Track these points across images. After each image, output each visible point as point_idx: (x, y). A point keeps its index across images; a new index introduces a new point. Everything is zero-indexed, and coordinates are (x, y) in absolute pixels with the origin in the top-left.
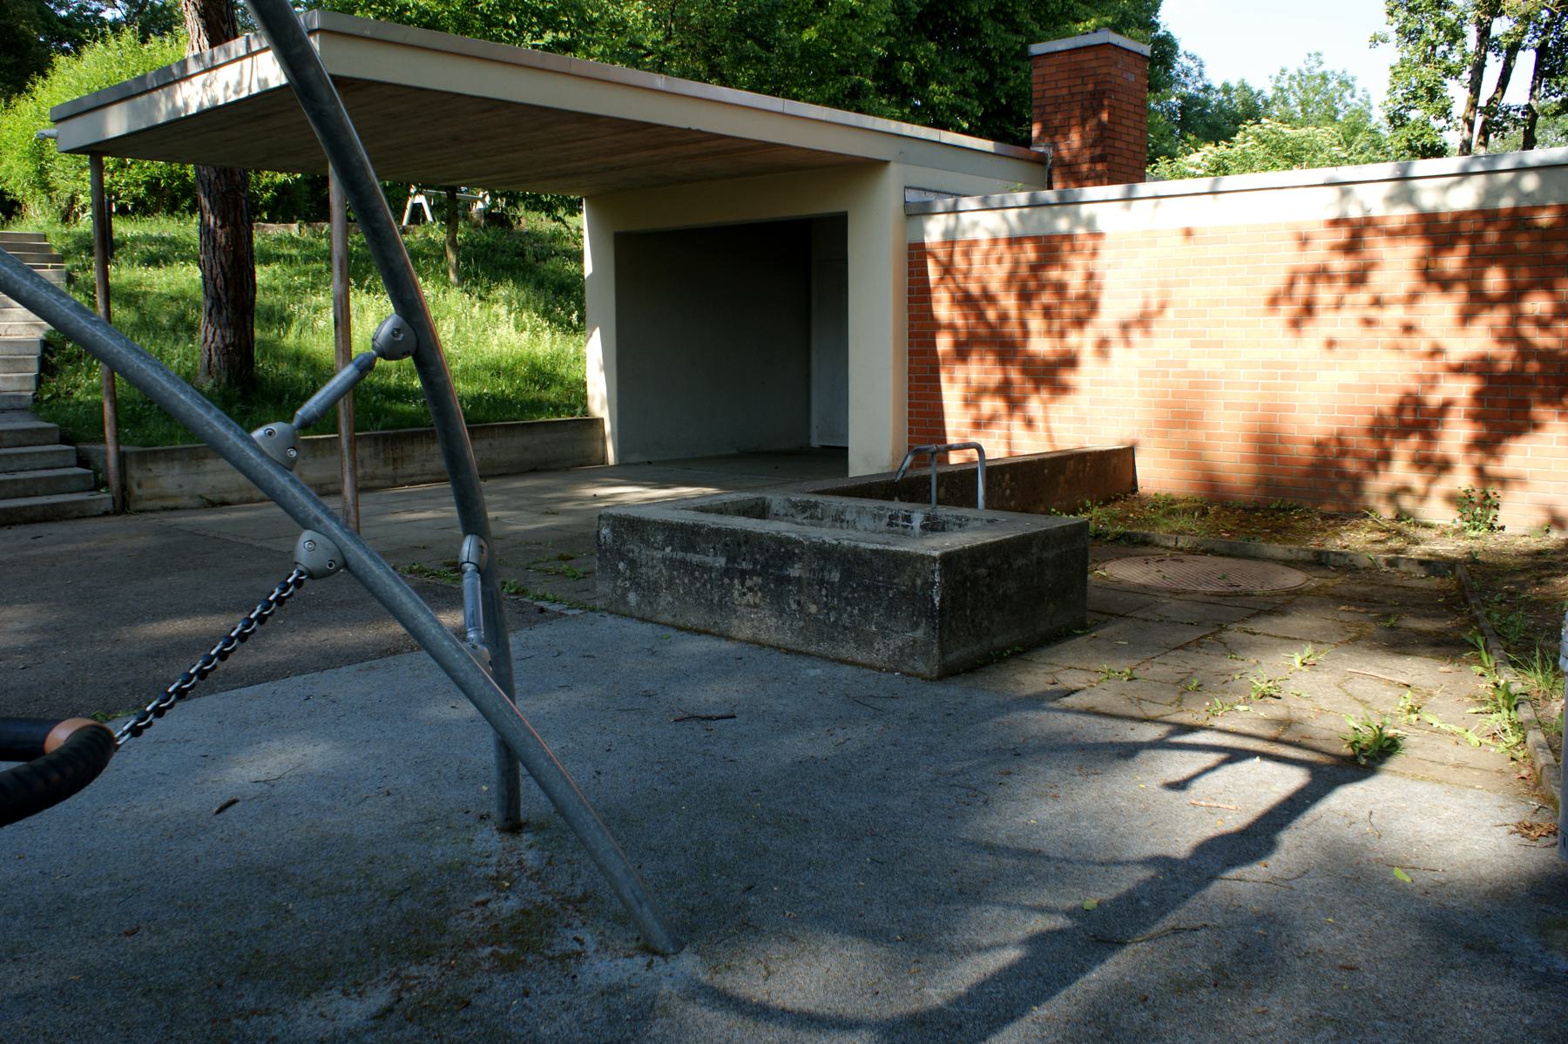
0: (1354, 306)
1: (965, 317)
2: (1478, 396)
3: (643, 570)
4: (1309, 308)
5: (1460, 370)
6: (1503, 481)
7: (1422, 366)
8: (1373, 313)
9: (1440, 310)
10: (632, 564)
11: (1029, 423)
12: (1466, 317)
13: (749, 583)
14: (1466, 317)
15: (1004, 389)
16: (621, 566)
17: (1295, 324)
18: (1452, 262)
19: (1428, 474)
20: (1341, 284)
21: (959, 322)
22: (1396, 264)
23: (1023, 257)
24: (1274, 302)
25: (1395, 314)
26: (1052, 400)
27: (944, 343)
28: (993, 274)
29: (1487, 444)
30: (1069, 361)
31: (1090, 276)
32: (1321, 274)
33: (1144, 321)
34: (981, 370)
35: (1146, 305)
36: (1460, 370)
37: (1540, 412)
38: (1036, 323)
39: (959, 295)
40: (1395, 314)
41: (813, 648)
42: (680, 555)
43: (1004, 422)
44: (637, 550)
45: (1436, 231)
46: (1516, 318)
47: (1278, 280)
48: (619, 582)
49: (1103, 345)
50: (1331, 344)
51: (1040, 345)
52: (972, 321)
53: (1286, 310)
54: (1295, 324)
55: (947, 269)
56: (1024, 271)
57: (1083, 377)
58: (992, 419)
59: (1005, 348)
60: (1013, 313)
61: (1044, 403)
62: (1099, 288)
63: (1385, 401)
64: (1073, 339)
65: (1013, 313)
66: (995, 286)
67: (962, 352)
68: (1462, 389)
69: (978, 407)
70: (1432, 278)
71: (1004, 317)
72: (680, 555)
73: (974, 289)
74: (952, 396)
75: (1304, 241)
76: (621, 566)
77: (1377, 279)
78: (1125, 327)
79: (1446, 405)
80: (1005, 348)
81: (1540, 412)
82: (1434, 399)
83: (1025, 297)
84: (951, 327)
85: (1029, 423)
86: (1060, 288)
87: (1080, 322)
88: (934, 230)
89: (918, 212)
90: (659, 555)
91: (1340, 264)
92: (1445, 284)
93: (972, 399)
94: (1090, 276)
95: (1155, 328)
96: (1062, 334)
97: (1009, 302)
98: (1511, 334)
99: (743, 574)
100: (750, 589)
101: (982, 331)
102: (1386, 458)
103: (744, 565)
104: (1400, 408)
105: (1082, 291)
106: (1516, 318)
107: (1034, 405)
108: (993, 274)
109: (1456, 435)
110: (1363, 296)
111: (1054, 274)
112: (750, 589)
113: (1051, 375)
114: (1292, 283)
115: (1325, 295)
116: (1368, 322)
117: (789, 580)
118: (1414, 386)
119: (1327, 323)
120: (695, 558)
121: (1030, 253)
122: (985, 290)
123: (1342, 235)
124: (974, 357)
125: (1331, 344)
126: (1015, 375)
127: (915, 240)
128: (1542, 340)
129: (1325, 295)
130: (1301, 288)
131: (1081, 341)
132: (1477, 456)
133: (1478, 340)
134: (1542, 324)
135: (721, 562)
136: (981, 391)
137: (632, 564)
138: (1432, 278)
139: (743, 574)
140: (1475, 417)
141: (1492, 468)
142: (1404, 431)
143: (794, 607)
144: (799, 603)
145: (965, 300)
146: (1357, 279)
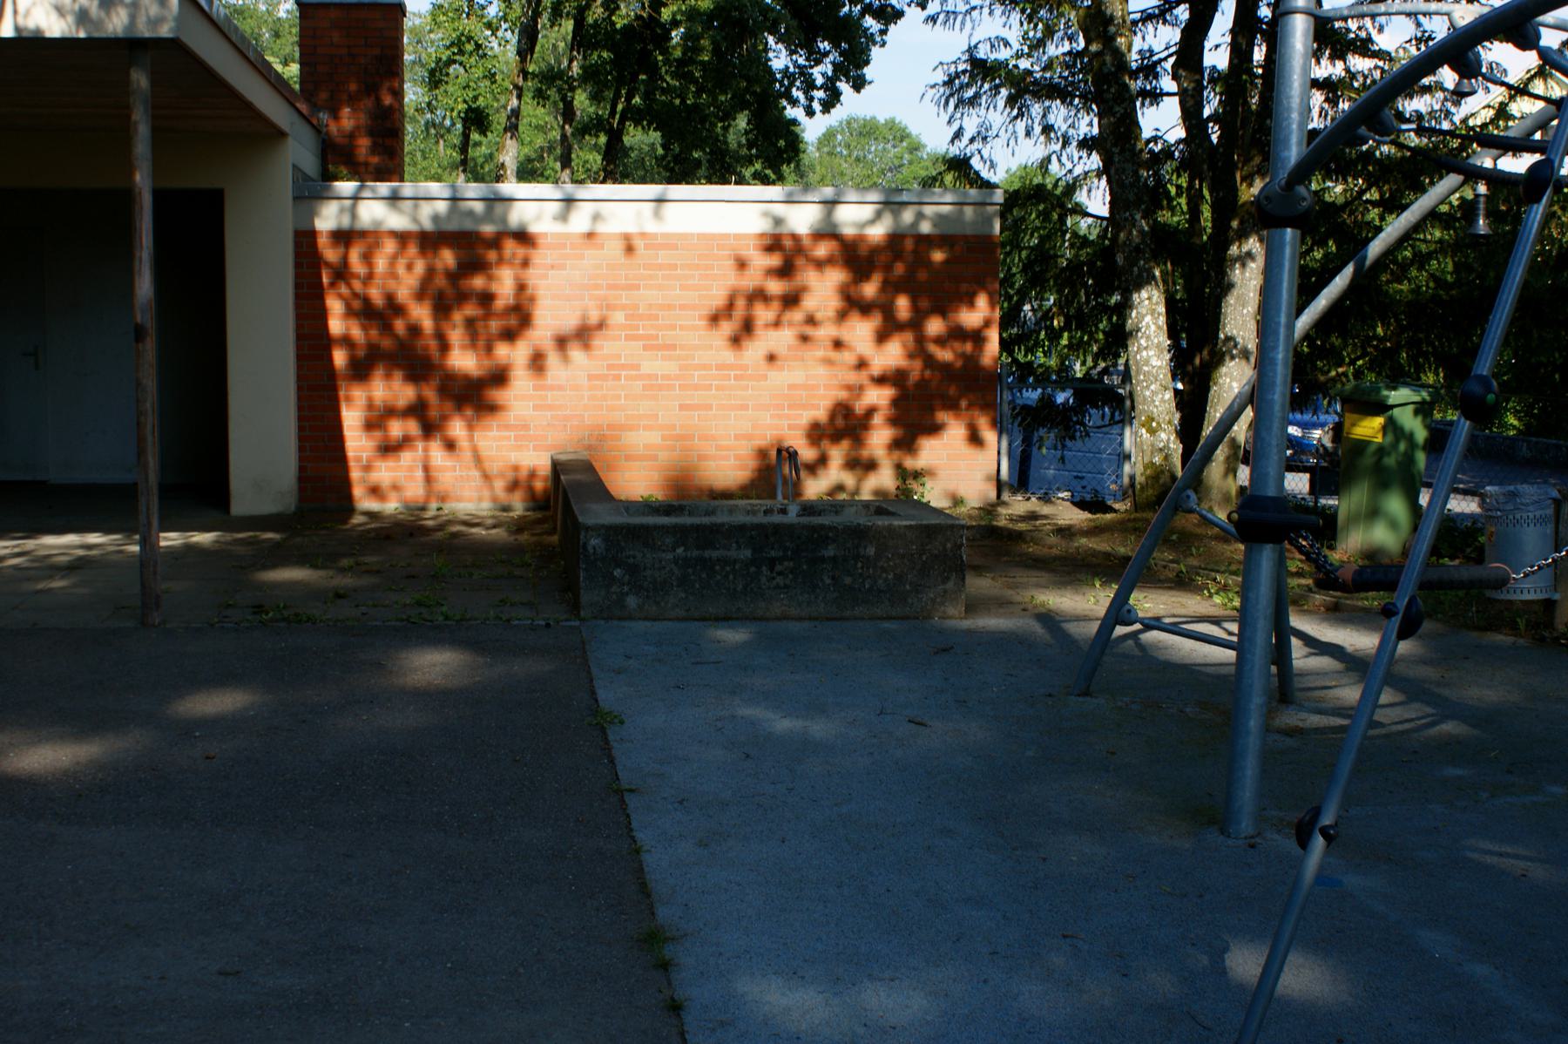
0: (791, 324)
1: (364, 328)
2: (895, 402)
3: (648, 573)
4: (748, 327)
5: (881, 380)
6: (917, 475)
7: (853, 377)
8: (809, 331)
9: (861, 331)
10: (633, 570)
11: (450, 445)
12: (882, 337)
13: (778, 568)
14: (882, 337)
15: (417, 410)
16: (617, 573)
17: (736, 341)
18: (870, 289)
19: (859, 472)
20: (776, 305)
21: (357, 333)
22: (823, 288)
23: (439, 265)
24: (715, 319)
25: (826, 332)
26: (479, 418)
27: (340, 358)
28: (402, 277)
29: (905, 443)
30: (499, 377)
31: (521, 287)
32: (758, 296)
33: (584, 335)
34: (388, 389)
35: (584, 317)
36: (881, 380)
37: (942, 416)
38: (456, 336)
39: (357, 304)
40: (826, 332)
41: (848, 613)
42: (695, 553)
43: (420, 445)
44: (639, 555)
45: (855, 258)
46: (921, 339)
47: (718, 298)
48: (614, 588)
49: (537, 362)
50: (771, 358)
51: (463, 360)
52: (374, 332)
53: (727, 328)
54: (736, 341)
55: (342, 273)
56: (440, 282)
57: (519, 395)
58: (405, 443)
59: (415, 361)
60: (427, 324)
61: (470, 428)
62: (532, 299)
63: (820, 412)
64: (502, 351)
65: (427, 324)
66: (404, 293)
67: (361, 370)
68: (879, 397)
69: (385, 429)
70: (852, 304)
71: (415, 330)
72: (695, 553)
73: (376, 295)
74: (352, 418)
75: (742, 264)
76: (617, 573)
77: (809, 303)
78: (562, 342)
79: (871, 411)
80: (415, 361)
81: (942, 416)
82: (860, 407)
83: (442, 309)
84: (347, 341)
85: (450, 445)
86: (487, 298)
87: (510, 335)
88: (328, 218)
89: (312, 192)
90: (670, 556)
91: (775, 287)
92: (865, 308)
93: (376, 421)
94: (521, 287)
95: (596, 342)
96: (489, 349)
97: (422, 314)
98: (919, 350)
99: (772, 563)
100: (780, 574)
101: (386, 343)
102: (823, 461)
103: (773, 553)
104: (832, 416)
105: (511, 301)
106: (921, 339)
107: (457, 428)
108: (402, 277)
109: (879, 438)
110: (797, 315)
111: (478, 282)
112: (780, 574)
113: (477, 396)
114: (730, 306)
115: (763, 314)
116: (805, 339)
117: (823, 559)
118: (843, 395)
119: (768, 340)
120: (715, 554)
121: (448, 258)
122: (390, 298)
123: (775, 260)
124: (379, 373)
125: (771, 358)
126: (430, 394)
127: (304, 227)
128: (945, 355)
129: (763, 314)
130: (739, 311)
131: (515, 354)
132: (897, 454)
133: (893, 355)
134: (940, 341)
135: (748, 553)
136: (390, 412)
137: (633, 570)
138: (852, 304)
139: (772, 563)
140: (893, 421)
141: (910, 463)
142: (836, 437)
143: (828, 581)
144: (833, 578)
145: (364, 311)
146: (791, 300)
